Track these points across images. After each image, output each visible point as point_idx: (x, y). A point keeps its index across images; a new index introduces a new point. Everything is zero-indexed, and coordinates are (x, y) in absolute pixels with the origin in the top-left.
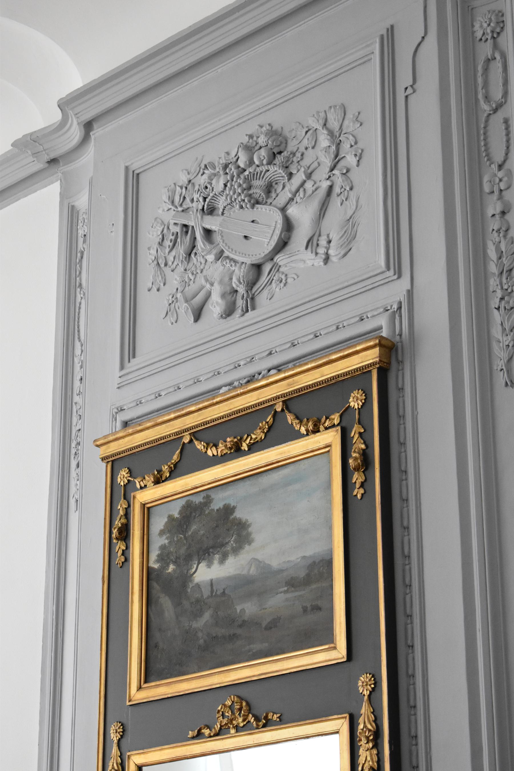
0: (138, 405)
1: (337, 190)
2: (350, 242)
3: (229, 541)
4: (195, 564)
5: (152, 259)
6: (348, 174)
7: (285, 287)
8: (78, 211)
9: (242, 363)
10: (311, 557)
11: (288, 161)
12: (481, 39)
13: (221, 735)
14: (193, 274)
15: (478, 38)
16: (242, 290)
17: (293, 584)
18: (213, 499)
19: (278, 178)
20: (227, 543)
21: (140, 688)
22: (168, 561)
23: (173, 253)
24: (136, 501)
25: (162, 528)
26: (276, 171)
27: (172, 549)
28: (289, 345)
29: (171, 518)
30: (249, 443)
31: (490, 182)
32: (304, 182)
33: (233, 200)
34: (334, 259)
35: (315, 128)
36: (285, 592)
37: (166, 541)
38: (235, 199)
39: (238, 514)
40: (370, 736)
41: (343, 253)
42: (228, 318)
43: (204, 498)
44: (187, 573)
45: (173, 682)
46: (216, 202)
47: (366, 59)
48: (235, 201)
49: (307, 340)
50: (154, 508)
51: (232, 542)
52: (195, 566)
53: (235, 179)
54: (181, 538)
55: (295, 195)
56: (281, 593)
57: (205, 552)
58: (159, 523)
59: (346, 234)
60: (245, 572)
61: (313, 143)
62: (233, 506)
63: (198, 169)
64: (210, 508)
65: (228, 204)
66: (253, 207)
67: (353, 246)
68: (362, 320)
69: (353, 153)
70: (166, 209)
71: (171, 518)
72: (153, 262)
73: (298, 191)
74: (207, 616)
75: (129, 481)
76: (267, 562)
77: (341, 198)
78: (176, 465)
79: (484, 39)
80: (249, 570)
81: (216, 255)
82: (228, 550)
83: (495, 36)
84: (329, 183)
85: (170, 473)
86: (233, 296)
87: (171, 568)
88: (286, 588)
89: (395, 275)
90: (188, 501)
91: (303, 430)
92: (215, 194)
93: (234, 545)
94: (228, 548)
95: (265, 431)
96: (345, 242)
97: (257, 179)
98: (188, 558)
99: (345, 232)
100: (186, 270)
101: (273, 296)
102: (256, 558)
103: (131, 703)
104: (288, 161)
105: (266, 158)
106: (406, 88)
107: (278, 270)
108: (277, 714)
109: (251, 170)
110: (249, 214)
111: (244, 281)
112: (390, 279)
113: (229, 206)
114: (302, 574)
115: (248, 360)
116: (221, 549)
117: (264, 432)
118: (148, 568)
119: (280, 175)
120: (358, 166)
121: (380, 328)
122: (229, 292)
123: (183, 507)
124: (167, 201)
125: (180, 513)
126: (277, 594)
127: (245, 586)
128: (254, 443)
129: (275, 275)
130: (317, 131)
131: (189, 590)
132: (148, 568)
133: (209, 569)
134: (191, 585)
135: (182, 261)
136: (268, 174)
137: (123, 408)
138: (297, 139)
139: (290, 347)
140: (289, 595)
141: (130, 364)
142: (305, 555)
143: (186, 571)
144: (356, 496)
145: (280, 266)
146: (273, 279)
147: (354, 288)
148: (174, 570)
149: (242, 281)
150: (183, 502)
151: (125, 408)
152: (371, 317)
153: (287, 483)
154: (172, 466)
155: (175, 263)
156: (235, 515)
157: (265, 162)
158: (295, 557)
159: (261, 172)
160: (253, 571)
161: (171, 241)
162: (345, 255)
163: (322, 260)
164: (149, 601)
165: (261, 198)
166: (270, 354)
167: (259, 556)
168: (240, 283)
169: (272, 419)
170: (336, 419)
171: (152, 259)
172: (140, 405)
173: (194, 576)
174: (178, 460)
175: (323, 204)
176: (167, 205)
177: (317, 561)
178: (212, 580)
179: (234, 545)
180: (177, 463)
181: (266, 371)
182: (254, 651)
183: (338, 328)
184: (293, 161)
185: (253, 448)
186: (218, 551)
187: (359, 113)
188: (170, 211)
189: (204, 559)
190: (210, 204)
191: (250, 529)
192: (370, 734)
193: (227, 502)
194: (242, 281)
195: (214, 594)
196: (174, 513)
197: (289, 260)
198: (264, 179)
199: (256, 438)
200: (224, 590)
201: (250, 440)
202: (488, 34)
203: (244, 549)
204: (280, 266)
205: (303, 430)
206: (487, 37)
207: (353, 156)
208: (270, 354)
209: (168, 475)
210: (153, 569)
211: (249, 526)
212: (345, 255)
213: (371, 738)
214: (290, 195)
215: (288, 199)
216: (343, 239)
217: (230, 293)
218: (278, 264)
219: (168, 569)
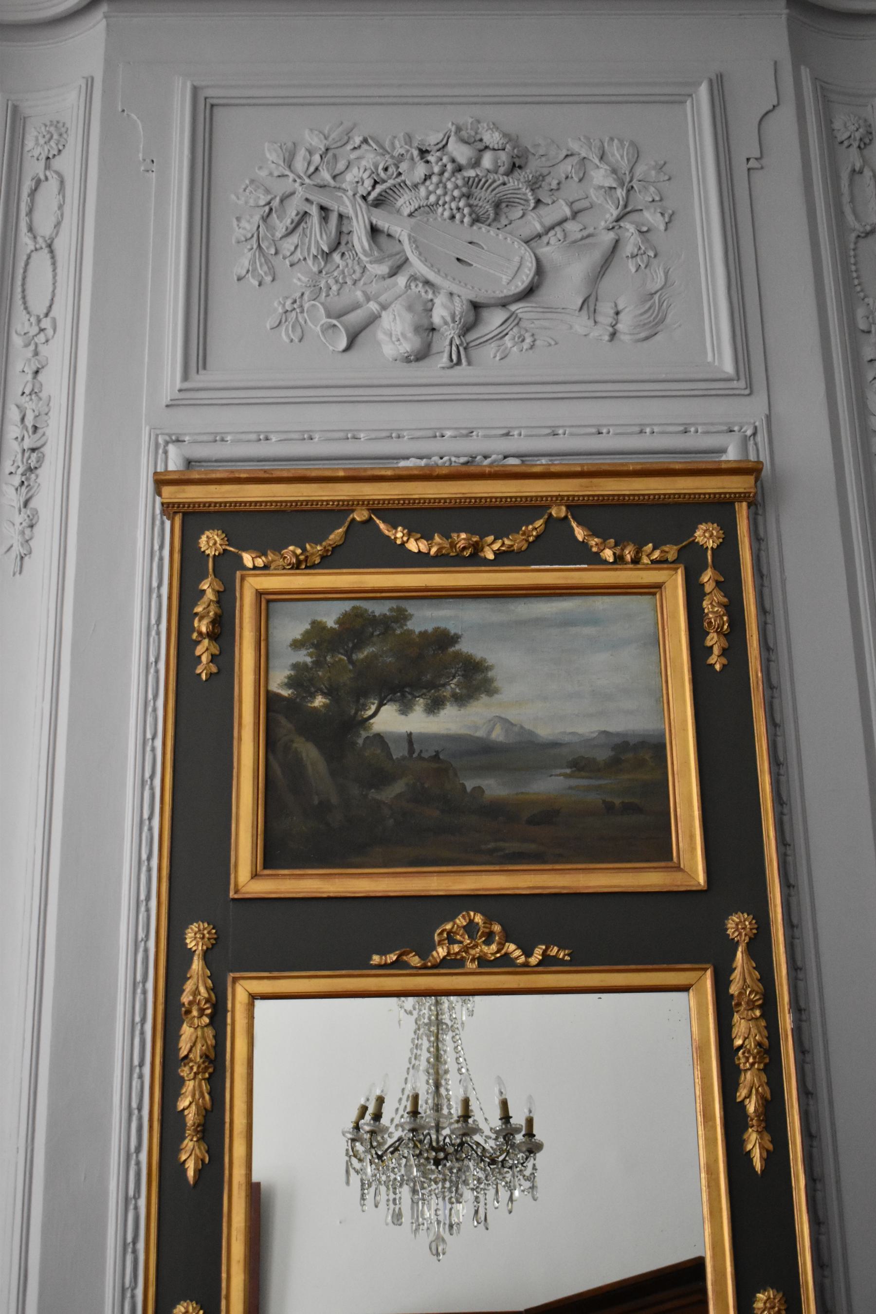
0: (435, 437)
1: (629, 248)
2: (656, 324)
3: (448, 684)
4: (373, 704)
5: (245, 237)
6: (648, 235)
7: (531, 352)
8: (25, 118)
9: (448, 433)
10: (618, 734)
11: (535, 183)
12: (842, 143)
13: (443, 968)
14: (337, 282)
15: (839, 140)
16: (450, 332)
17: (580, 765)
18: (411, 616)
19: (517, 200)
20: (444, 685)
21: (255, 875)
22: (313, 689)
23: (294, 239)
24: (246, 585)
25: (299, 637)
26: (519, 189)
27: (320, 673)
28: (594, 430)
29: (317, 627)
30: (498, 550)
31: (868, 318)
32: (565, 220)
33: (441, 202)
34: (625, 338)
35: (584, 155)
36: (566, 776)
37: (309, 660)
38: (445, 203)
39: (465, 647)
40: (207, 1009)
41: (643, 335)
42: (421, 363)
43: (391, 610)
44: (356, 713)
45: (336, 874)
46: (395, 196)
47: (677, 98)
48: (444, 205)
49: (715, 430)
50: (279, 604)
51: (453, 686)
52: (373, 708)
53: (446, 175)
54: (341, 660)
55: (547, 233)
56: (560, 775)
57: (400, 690)
58: (290, 628)
59: (651, 311)
60: (480, 733)
61: (581, 175)
62: (455, 634)
63: (346, 138)
64: (405, 628)
65: (427, 205)
66: (472, 224)
67: (662, 330)
68: (731, 431)
69: (659, 210)
70: (276, 174)
71: (317, 627)
72: (246, 240)
73: (552, 228)
74: (398, 787)
75: (224, 550)
76: (527, 726)
77: (637, 262)
78: (335, 548)
79: (846, 143)
80: (490, 732)
81: (391, 268)
82: (444, 696)
83: (862, 146)
84: (611, 235)
85: (323, 557)
86: (428, 335)
87: (319, 701)
88: (568, 771)
89: (746, 388)
90: (354, 608)
91: (608, 554)
92: (404, 182)
93: (458, 691)
94: (447, 692)
95: (531, 539)
96: (650, 322)
97: (482, 188)
98: (361, 694)
99: (650, 308)
100: (320, 272)
101: (506, 357)
102: (503, 716)
103: (236, 896)
104: (535, 183)
105: (506, 166)
106: (748, 160)
107: (518, 324)
108: (565, 949)
109: (471, 173)
110: (464, 230)
111: (460, 319)
112: (737, 392)
113: (427, 208)
114: (603, 755)
115: (464, 432)
116: (429, 691)
117: (527, 541)
118: (268, 692)
119: (523, 197)
120: (666, 229)
121: (724, 451)
122: (426, 327)
123: (346, 615)
124: (282, 164)
125: (339, 622)
126: (551, 776)
127: (483, 753)
128: (504, 552)
129: (512, 329)
130: (586, 161)
131: (360, 741)
132: (268, 692)
133: (403, 717)
134: (364, 734)
135: (315, 257)
136: (502, 188)
137: (180, 439)
138: (548, 160)
139: (548, 435)
140: (573, 782)
141: (198, 377)
142: (608, 729)
143: (353, 712)
144: (200, 674)
145: (520, 319)
146: (507, 334)
147: (610, 387)
148: (325, 706)
149: (457, 319)
150: (347, 606)
151: (187, 438)
152: (526, 436)
153: (567, 622)
154: (330, 548)
155: (298, 255)
156: (458, 647)
157: (502, 170)
158: (588, 728)
159: (494, 181)
160: (498, 735)
161: (292, 222)
162: (647, 338)
163: (608, 333)
164: (271, 743)
165: (485, 216)
166: (507, 434)
167: (512, 715)
168: (454, 321)
169: (543, 526)
170: (672, 552)
171: (245, 237)
172: (219, 443)
173: (372, 721)
174: (341, 543)
175: (607, 260)
176: (281, 168)
177: (632, 743)
178: (411, 733)
179: (458, 691)
180: (337, 546)
181: (501, 457)
182: (507, 852)
183: (641, 432)
184: (540, 186)
185: (504, 558)
186: (424, 694)
187: (665, 163)
188: (282, 179)
189: (391, 700)
190: (384, 194)
191: (490, 674)
192: (757, 997)
193: (443, 625)
194: (457, 319)
195: (415, 755)
196: (324, 620)
197: (541, 316)
198: (494, 192)
199: (512, 546)
200: (437, 753)
201: (502, 546)
202: (855, 140)
203: (478, 699)
204: (520, 319)
205: (608, 554)
206: (852, 142)
207: (659, 215)
208: (507, 434)
209: (317, 561)
210: (278, 695)
211: (489, 668)
212: (647, 338)
213: (209, 1011)
214: (539, 228)
215: (535, 233)
216: (646, 316)
217: (426, 329)
218: (517, 316)
219: (312, 702)
